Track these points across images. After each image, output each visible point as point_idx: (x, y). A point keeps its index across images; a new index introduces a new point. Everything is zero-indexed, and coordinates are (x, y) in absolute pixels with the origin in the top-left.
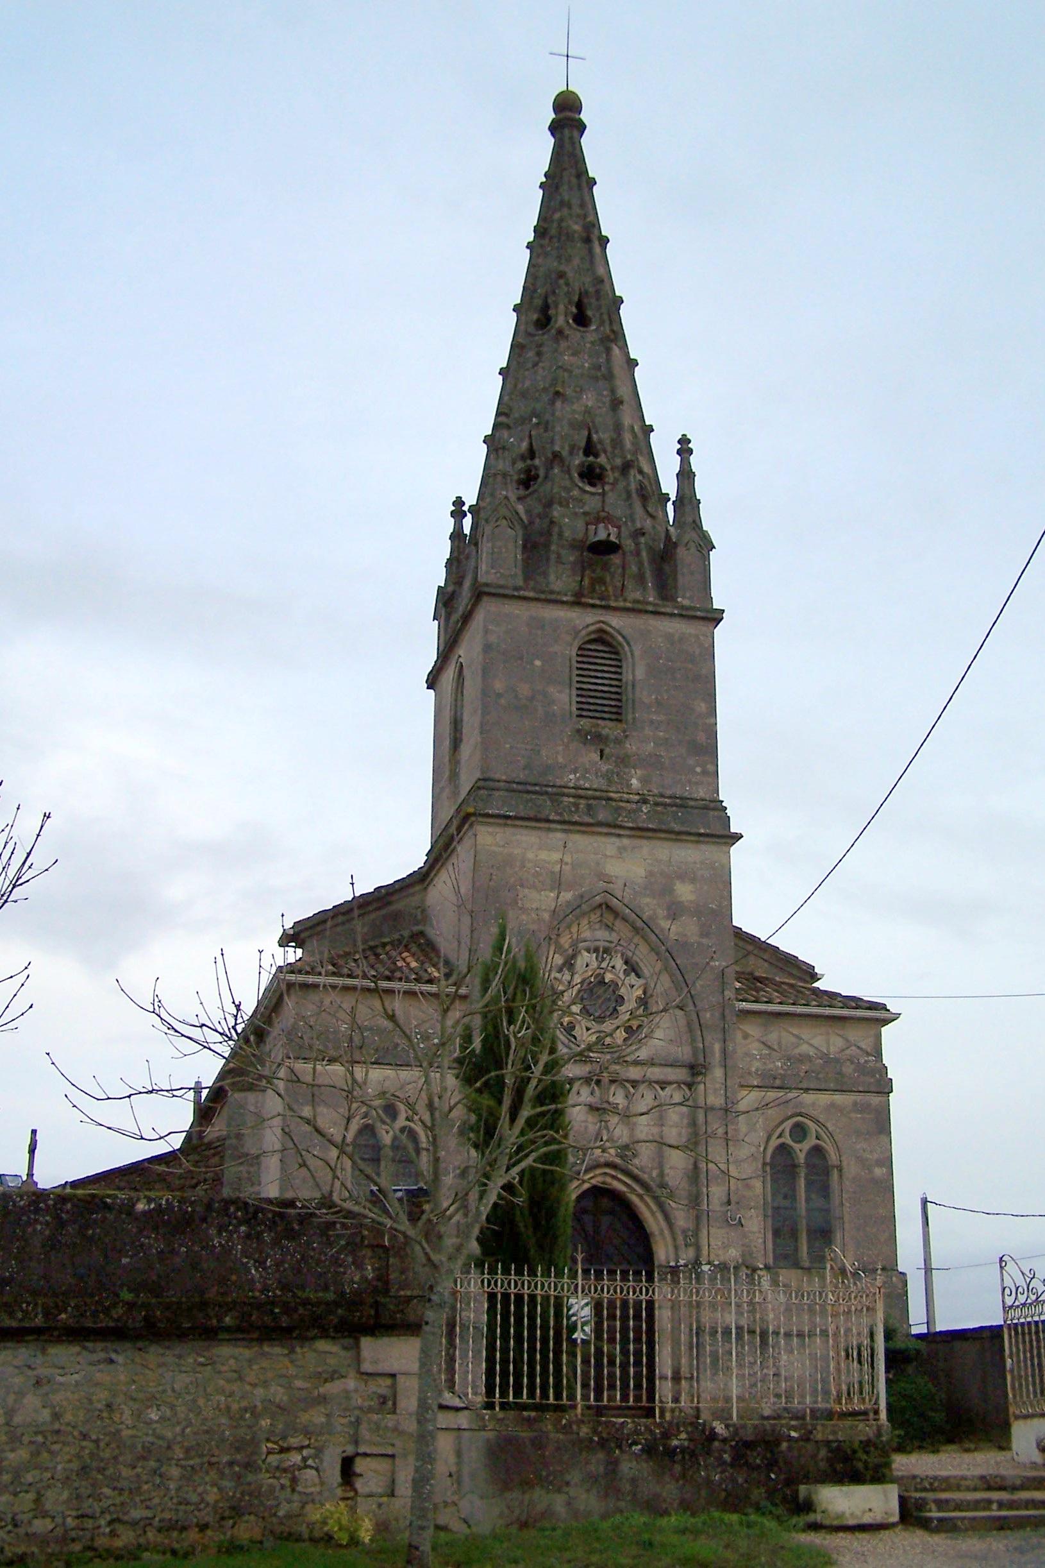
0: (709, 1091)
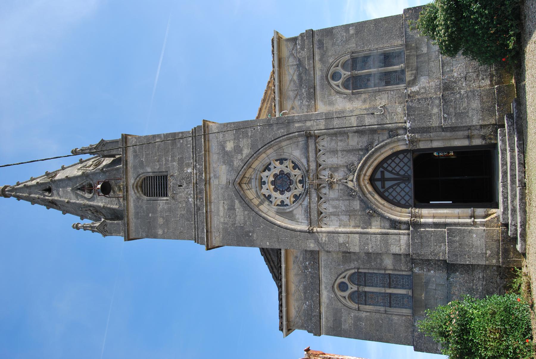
0: (318, 127)
